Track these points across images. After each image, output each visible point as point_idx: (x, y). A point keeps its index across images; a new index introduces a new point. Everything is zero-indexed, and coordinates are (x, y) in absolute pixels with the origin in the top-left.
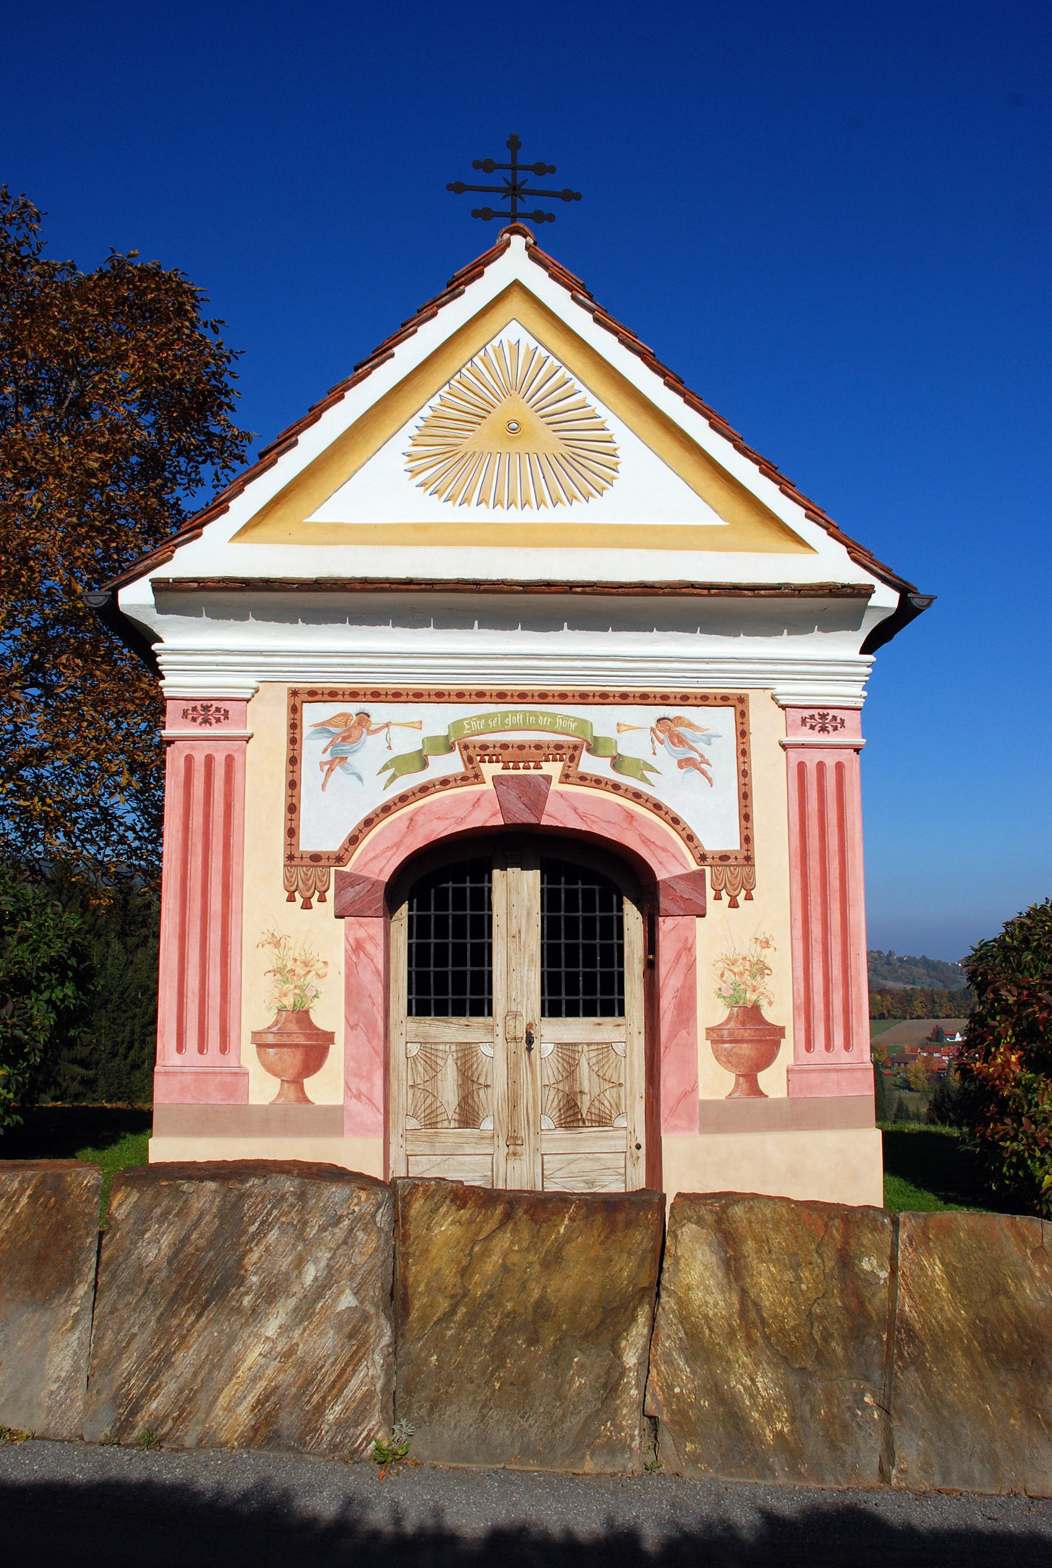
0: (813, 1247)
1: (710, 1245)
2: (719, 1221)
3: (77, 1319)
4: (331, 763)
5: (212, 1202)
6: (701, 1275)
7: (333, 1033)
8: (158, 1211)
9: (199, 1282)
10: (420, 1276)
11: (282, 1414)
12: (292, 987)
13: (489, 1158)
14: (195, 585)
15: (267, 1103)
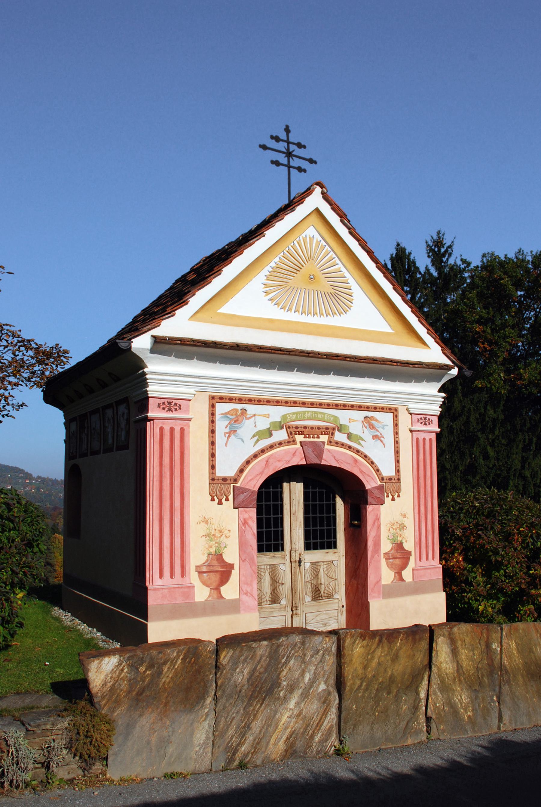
0: (478, 641)
1: (447, 645)
2: (449, 634)
3: (207, 715)
4: (229, 433)
5: (266, 650)
6: (445, 657)
7: (234, 564)
8: (242, 658)
9: (261, 689)
10: (349, 672)
11: (297, 742)
12: (214, 543)
13: (284, 617)
14: (179, 342)
15: (203, 600)
